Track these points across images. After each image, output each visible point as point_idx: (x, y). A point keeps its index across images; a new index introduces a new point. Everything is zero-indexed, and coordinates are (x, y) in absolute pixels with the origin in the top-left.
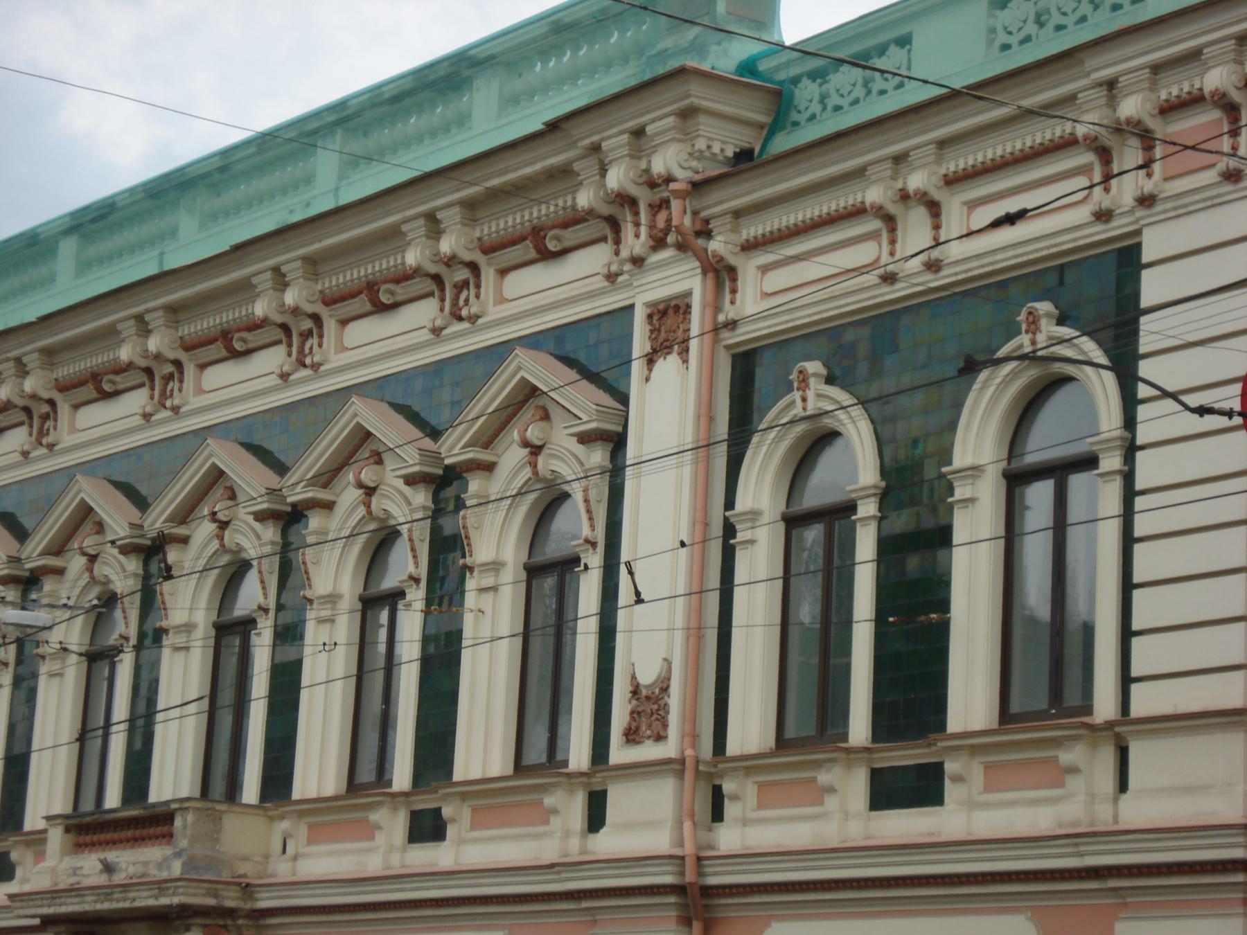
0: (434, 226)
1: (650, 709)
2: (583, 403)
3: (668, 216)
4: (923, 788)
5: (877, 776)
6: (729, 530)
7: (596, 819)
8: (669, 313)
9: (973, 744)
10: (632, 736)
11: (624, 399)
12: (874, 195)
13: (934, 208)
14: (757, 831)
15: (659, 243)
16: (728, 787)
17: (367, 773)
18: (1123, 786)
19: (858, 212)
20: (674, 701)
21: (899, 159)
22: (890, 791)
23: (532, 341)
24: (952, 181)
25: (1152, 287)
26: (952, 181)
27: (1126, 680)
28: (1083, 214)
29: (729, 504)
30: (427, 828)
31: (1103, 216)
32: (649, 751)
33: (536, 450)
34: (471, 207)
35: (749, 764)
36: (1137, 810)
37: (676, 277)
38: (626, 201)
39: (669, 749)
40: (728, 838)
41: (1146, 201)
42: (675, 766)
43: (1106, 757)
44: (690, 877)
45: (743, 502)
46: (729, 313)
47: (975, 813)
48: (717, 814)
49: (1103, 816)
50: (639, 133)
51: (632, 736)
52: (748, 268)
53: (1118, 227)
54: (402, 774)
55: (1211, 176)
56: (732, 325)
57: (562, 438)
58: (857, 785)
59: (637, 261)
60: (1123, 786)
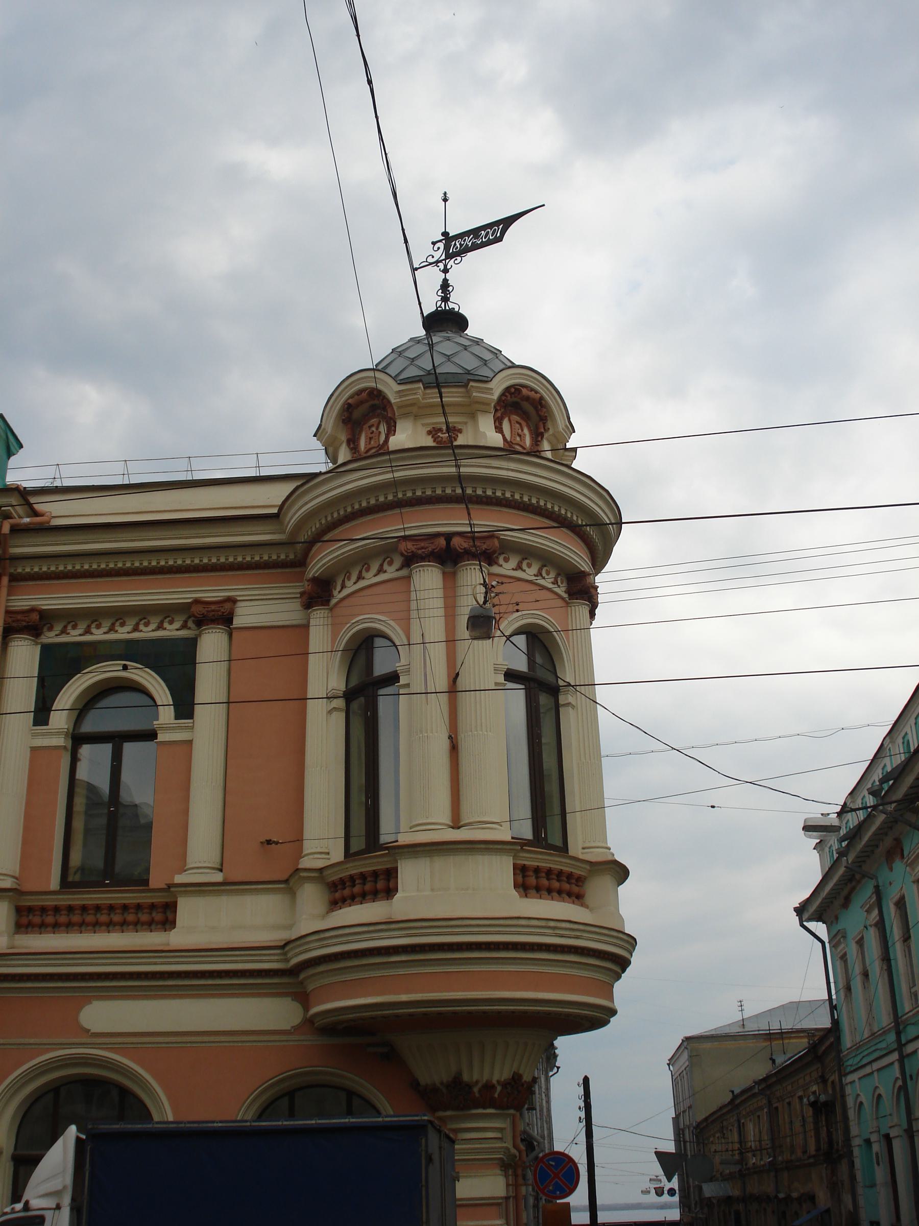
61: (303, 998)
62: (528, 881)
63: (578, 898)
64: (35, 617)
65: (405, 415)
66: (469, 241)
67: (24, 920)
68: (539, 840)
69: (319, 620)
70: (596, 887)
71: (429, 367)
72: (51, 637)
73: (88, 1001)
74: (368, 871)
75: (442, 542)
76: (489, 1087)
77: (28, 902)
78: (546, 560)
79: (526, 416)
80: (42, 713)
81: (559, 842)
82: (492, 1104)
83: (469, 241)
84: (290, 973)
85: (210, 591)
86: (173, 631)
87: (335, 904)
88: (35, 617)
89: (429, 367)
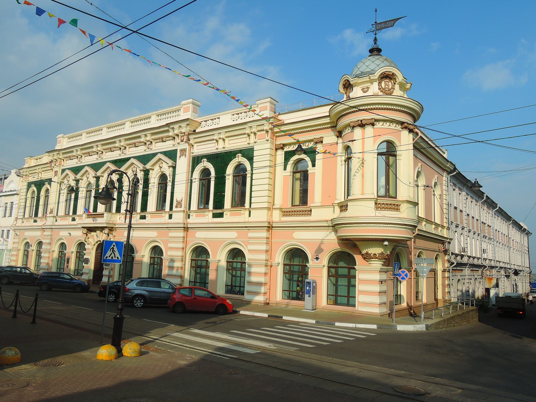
0: (120, 141)
1: (179, 204)
2: (170, 162)
3: (187, 137)
4: (221, 215)
5: (213, 214)
6: (191, 180)
7: (170, 217)
8: (183, 151)
9: (40, 218)
10: (176, 207)
11: (176, 162)
12: (215, 137)
13: (224, 140)
14: (194, 220)
15: (182, 141)
16: (191, 214)
17: (67, 213)
18: (250, 216)
19: (245, 134)
20: (183, 203)
21: (220, 133)
22: (215, 216)
23: (68, 169)
24: (227, 137)
25: (255, 153)
26: (227, 137)
27: (251, 203)
28: (246, 143)
29: (192, 177)
30: (35, 221)
31: (249, 144)
32: (51, 215)
33: (161, 167)
34: (103, 145)
35: (60, 217)
36: (251, 219)
37: (185, 146)
38: (178, 135)
39: (182, 209)
40: (189, 221)
41: (255, 142)
42: (54, 217)
43: (247, 212)
44: (186, 226)
45: (194, 177)
46: (192, 151)
47: (40, 223)
48: (189, 218)
49: (247, 220)
50: (180, 126)
51: (176, 207)
52: (195, 145)
53: (250, 145)
54: (71, 213)
55: (265, 140)
56: (193, 153)
57: (165, 166)
58: (211, 214)
59: (178, 143)
60: (250, 216)
61: (336, 231)
62: (378, 206)
63: (398, 210)
64: (282, 145)
65: (356, 86)
66: (383, 25)
67: (377, 206)
68: (387, 195)
69: (340, 140)
70: (322, 247)
71: (124, 240)
72: (287, 149)
73: (294, 232)
74: (343, 207)
75: (360, 122)
76: (375, 254)
77: (283, 210)
78: (392, 121)
79: (391, 79)
80: (285, 169)
81: (394, 196)
82: (376, 258)
83: (383, 25)
84: (335, 227)
85: (316, 135)
86: (311, 145)
87: (284, 215)
88: (282, 145)
89: (124, 240)
